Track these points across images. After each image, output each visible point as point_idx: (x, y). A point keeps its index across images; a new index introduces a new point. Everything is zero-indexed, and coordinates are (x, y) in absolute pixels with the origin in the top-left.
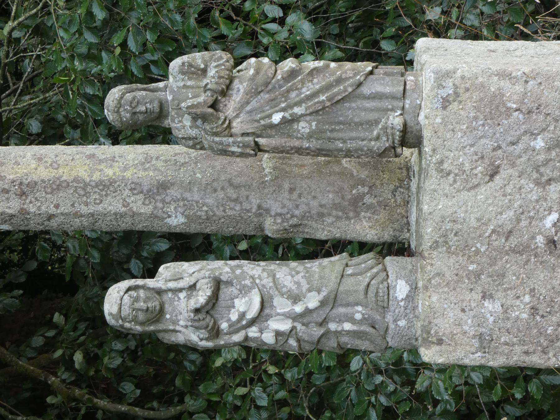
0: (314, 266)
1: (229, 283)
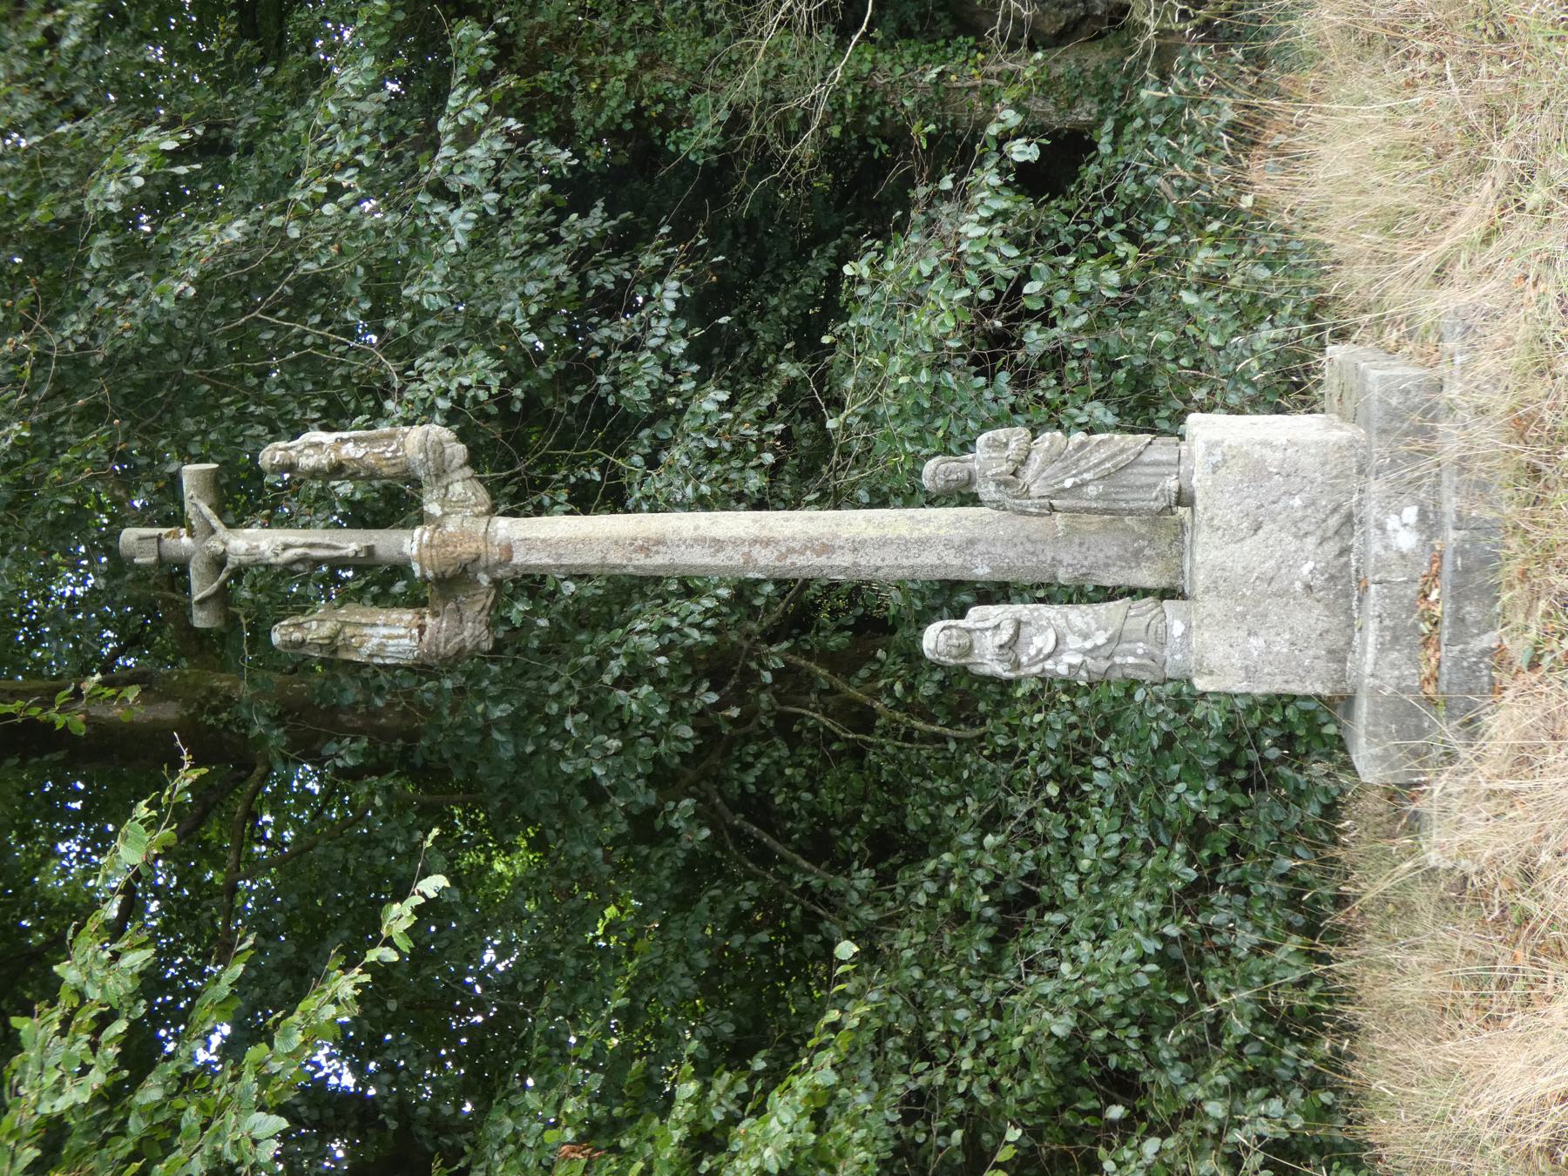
0: (1102, 608)
1: (1028, 623)
